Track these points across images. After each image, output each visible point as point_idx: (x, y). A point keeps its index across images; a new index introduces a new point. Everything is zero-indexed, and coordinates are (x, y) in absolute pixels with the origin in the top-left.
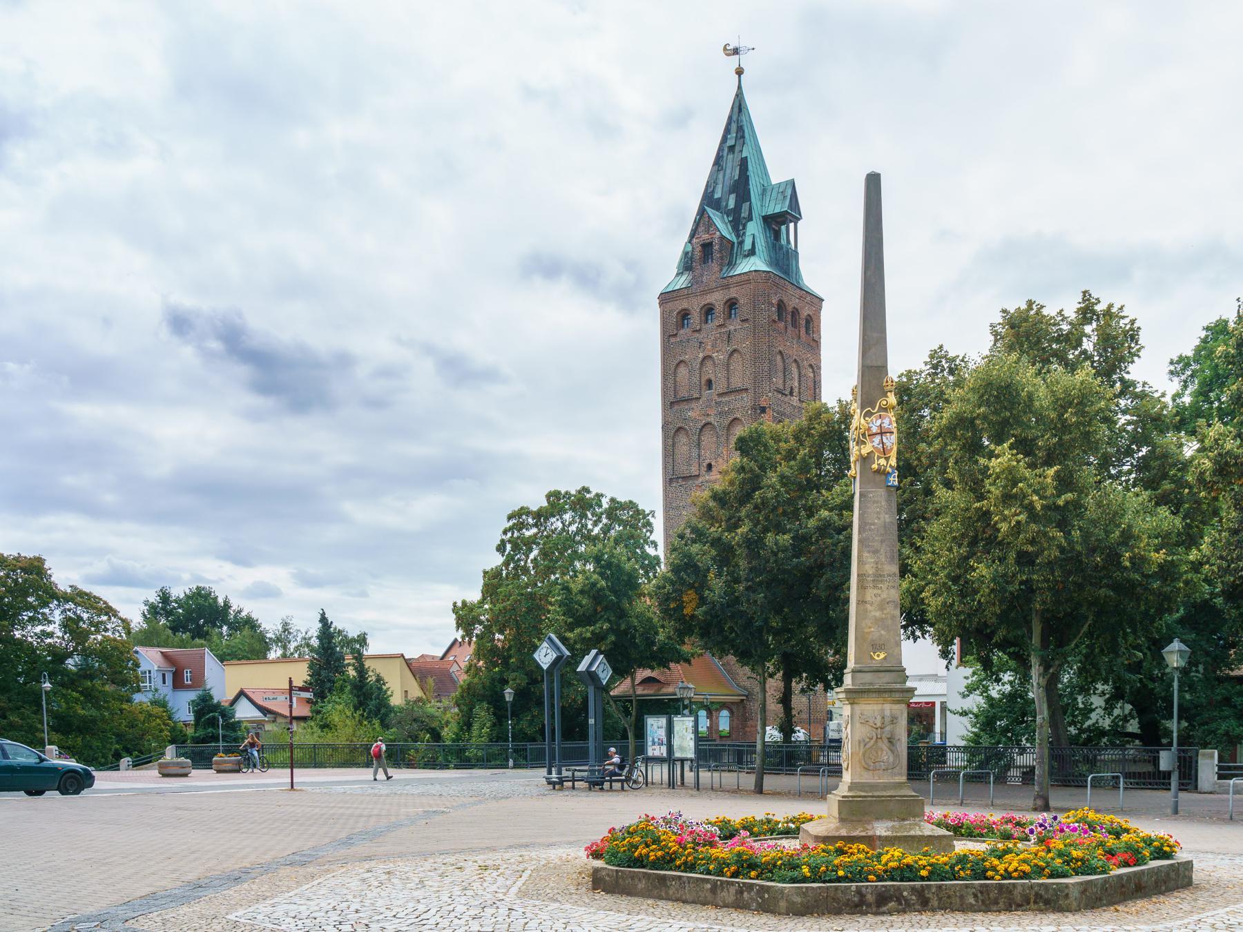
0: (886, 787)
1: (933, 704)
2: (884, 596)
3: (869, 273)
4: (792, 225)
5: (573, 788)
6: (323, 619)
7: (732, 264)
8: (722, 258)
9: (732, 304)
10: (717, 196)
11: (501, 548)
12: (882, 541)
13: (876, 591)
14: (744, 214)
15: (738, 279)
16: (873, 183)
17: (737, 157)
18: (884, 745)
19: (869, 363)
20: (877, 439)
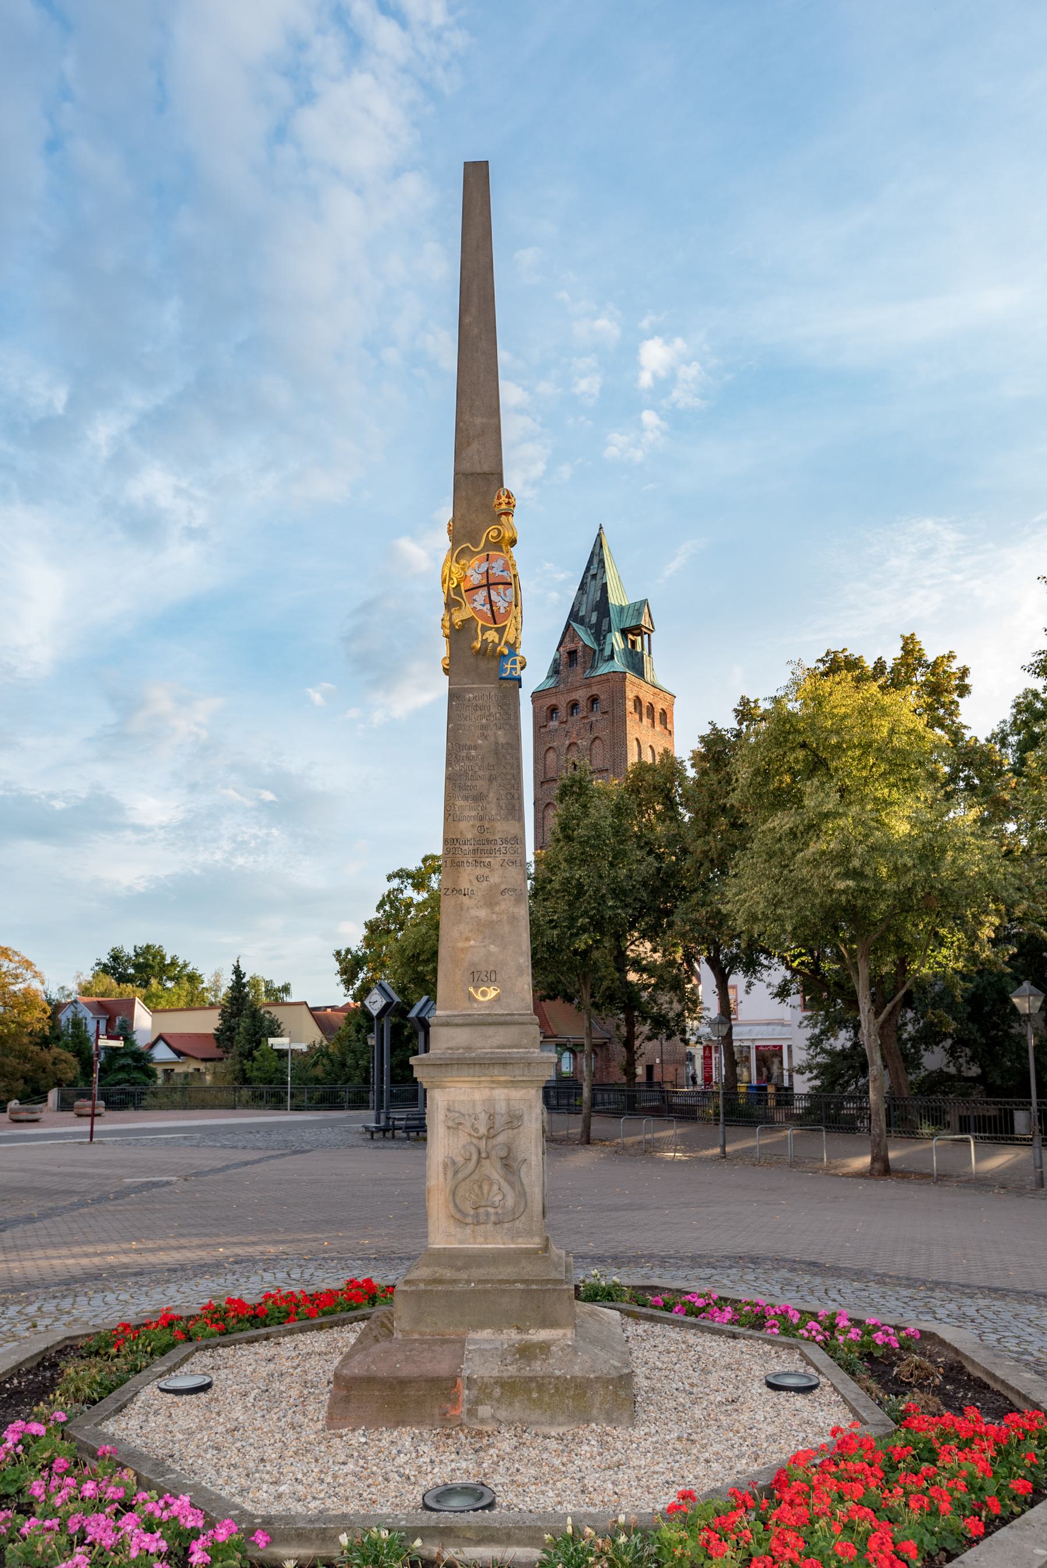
0: (496, 1258)
1: (781, 1047)
2: (495, 879)
3: (467, 320)
4: (646, 637)
5: (393, 1137)
6: (238, 972)
7: (593, 667)
8: (585, 662)
9: (594, 700)
10: (581, 614)
11: (381, 906)
12: (491, 779)
13: (479, 871)
14: (605, 627)
15: (595, 680)
16: (477, 178)
17: (599, 583)
18: (493, 1171)
19: (467, 467)
20: (481, 595)
